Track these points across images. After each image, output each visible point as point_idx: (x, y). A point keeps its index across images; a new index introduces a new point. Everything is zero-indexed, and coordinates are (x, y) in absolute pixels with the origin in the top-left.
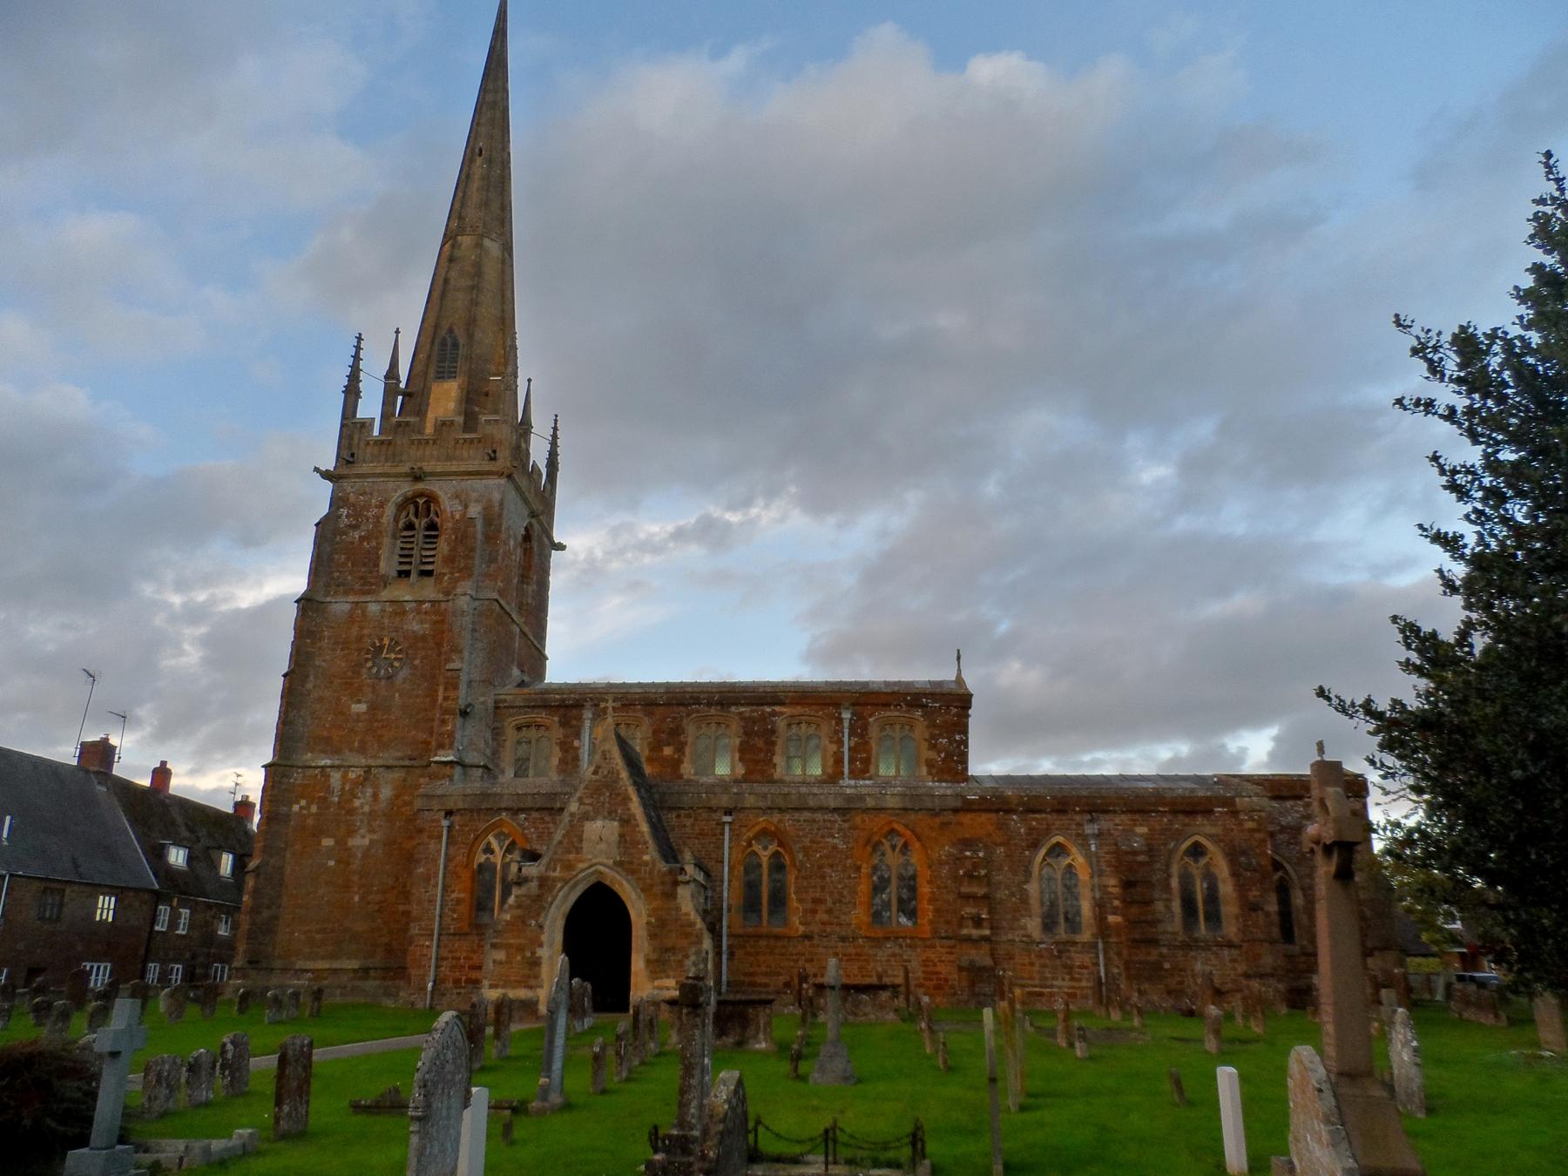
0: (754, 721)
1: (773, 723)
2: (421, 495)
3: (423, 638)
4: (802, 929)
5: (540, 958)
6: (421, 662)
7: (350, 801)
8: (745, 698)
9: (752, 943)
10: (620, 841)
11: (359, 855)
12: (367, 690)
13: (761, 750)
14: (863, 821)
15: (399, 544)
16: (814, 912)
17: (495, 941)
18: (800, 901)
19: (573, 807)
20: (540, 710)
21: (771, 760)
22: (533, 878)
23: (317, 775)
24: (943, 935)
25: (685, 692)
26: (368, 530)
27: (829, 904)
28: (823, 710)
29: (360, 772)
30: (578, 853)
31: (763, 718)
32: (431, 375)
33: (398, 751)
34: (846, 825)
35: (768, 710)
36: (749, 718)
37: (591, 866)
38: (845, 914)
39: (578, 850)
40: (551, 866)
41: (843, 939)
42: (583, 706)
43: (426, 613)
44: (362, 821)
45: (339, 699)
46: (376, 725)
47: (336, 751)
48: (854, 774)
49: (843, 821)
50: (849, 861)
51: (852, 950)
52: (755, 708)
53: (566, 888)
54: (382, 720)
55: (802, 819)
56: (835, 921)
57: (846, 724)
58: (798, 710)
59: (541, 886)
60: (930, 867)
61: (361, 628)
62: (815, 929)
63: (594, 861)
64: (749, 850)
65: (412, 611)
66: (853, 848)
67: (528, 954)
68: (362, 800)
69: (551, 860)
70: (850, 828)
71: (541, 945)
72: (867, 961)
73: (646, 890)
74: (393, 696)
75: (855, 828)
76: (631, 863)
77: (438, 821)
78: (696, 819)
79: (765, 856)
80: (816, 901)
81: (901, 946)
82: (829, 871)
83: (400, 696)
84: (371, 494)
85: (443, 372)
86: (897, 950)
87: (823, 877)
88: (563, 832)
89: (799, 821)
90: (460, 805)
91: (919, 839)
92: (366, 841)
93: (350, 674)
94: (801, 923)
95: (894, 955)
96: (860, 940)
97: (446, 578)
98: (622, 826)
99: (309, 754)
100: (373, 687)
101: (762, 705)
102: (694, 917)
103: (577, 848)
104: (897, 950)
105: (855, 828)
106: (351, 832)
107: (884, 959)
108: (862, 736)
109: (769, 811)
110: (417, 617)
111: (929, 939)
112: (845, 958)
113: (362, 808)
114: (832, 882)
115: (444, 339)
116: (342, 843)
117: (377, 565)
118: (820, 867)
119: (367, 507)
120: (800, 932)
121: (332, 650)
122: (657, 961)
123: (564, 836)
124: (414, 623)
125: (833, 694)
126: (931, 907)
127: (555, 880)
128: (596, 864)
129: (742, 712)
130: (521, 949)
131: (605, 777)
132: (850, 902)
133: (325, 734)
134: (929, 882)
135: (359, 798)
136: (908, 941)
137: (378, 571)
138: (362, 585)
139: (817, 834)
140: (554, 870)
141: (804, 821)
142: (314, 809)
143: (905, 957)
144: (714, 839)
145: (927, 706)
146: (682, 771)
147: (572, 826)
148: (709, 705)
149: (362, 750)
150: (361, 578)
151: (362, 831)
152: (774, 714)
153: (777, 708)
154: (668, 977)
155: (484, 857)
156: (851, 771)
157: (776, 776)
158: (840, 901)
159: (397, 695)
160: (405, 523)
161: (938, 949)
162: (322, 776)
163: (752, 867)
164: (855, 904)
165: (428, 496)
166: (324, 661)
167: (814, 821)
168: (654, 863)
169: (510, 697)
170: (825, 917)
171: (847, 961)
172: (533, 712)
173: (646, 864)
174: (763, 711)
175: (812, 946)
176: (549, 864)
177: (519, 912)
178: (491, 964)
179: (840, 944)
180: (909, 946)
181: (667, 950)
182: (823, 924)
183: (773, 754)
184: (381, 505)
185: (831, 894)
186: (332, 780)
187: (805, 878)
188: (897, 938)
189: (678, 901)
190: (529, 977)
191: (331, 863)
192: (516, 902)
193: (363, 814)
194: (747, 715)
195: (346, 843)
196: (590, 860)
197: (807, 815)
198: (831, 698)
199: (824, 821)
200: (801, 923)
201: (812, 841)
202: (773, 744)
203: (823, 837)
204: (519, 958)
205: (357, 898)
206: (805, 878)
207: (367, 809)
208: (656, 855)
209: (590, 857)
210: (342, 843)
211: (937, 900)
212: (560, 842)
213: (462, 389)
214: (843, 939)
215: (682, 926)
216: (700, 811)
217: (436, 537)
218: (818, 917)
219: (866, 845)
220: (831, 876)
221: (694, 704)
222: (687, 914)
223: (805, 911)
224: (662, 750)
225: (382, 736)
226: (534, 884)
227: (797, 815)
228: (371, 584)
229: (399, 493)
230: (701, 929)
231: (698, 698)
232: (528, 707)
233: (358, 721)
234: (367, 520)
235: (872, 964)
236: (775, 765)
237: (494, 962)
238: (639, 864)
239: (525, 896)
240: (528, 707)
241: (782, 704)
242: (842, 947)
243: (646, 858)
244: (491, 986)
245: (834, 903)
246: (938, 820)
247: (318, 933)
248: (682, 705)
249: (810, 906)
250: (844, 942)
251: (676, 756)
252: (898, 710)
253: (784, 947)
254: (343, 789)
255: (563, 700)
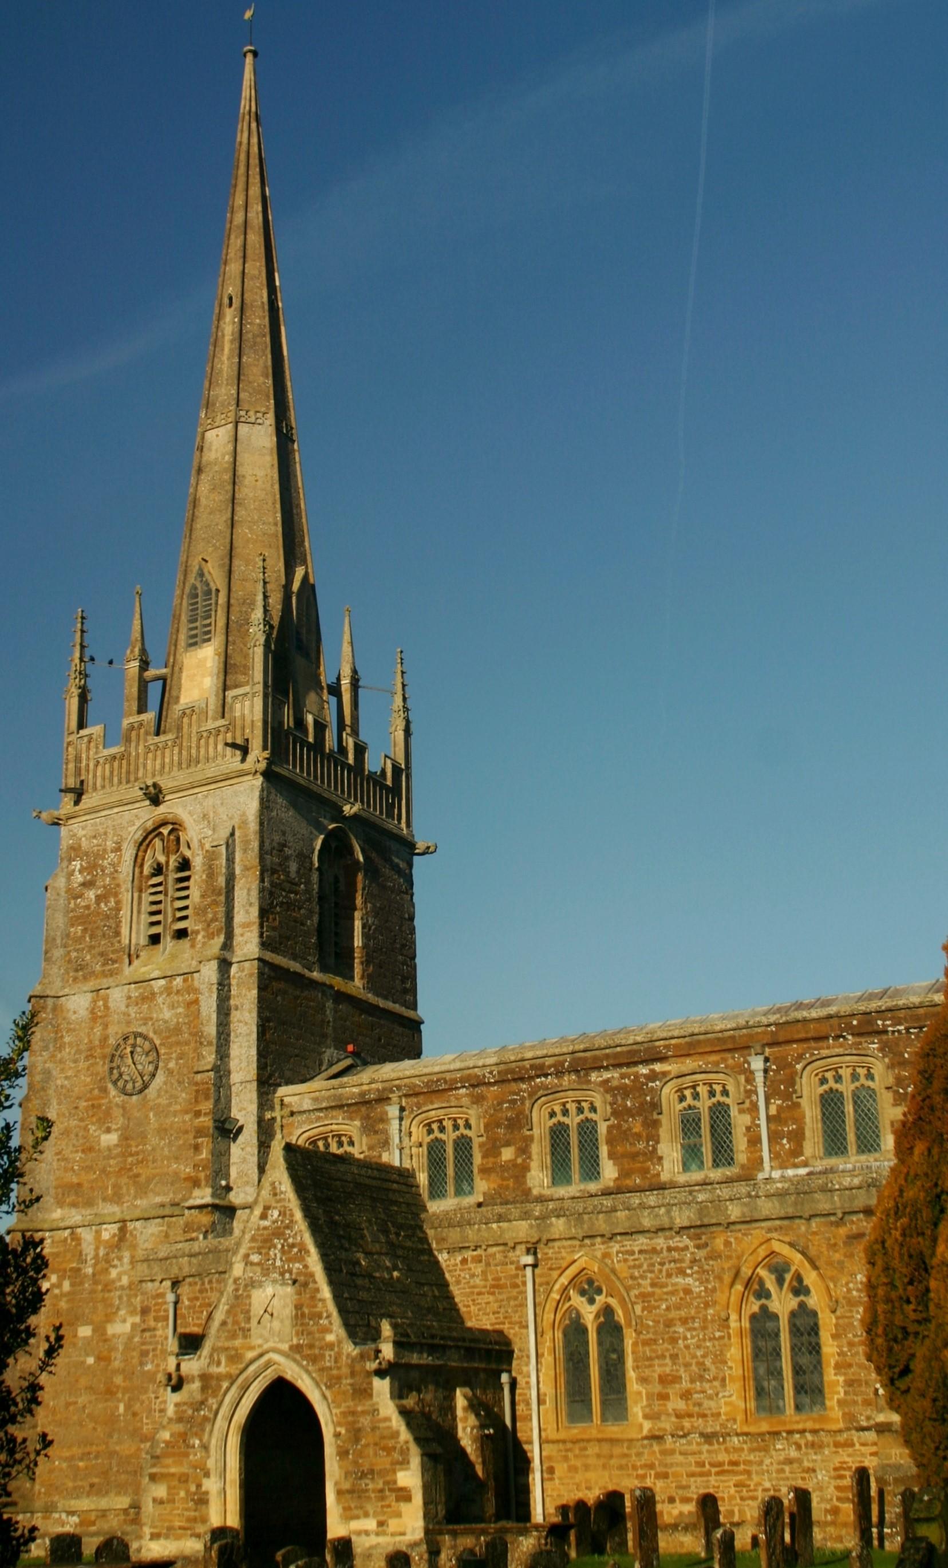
0: (624, 1091)
1: (656, 1093)
2: (164, 824)
3: (177, 1030)
4: (647, 1425)
5: (207, 1493)
6: (177, 1064)
7: (106, 1271)
8: (607, 1056)
9: (577, 1452)
10: (296, 1315)
11: (121, 1348)
12: (117, 1112)
13: (638, 1136)
14: (727, 1244)
15: (147, 898)
16: (664, 1397)
17: (154, 1470)
18: (643, 1380)
19: (238, 1269)
20: (334, 1113)
21: (655, 1149)
22: (193, 1377)
23: (66, 1239)
24: (864, 1424)
25: (523, 1060)
26: (104, 887)
27: (685, 1384)
28: (724, 1060)
29: (114, 1228)
30: (245, 1337)
31: (638, 1087)
32: (182, 637)
33: (159, 1194)
34: (701, 1254)
35: (644, 1070)
36: (617, 1088)
37: (261, 1355)
38: (710, 1398)
39: (246, 1332)
40: (214, 1361)
41: (708, 1438)
42: (389, 1099)
43: (178, 992)
44: (120, 1298)
45: (86, 1129)
46: (130, 1159)
47: (90, 1203)
48: (782, 1161)
49: (698, 1247)
50: (711, 1311)
51: (723, 1457)
52: (624, 1070)
53: (234, 1390)
54: (137, 1153)
55: (636, 1249)
56: (696, 1409)
57: (759, 1078)
58: (689, 1064)
59: (204, 1389)
60: (834, 1312)
61: (106, 1026)
62: (667, 1424)
63: (266, 1347)
64: (567, 1305)
65: (161, 993)
66: (714, 1290)
67: (193, 1488)
68: (119, 1269)
69: (214, 1350)
70: (708, 1258)
71: (207, 1475)
72: (749, 1473)
73: (332, 1382)
74: (147, 1116)
75: (714, 1256)
76: (311, 1346)
77: (162, 1295)
78: (488, 1264)
79: (589, 1314)
80: (663, 1380)
81: (799, 1447)
82: (681, 1330)
83: (154, 1116)
84: (105, 834)
85: (195, 636)
86: (793, 1453)
87: (674, 1340)
88: (226, 1307)
89: (632, 1253)
90: (186, 1271)
91: (815, 1267)
92: (127, 1327)
93: (96, 1092)
94: (646, 1417)
95: (789, 1461)
96: (735, 1439)
97: (200, 937)
98: (299, 1293)
99: (59, 1211)
100: (124, 1108)
101: (635, 1064)
102: (398, 1423)
103: (242, 1329)
104: (793, 1453)
105: (714, 1256)
106: (109, 1318)
107: (775, 1467)
108: (787, 1096)
109: (587, 1241)
110: (168, 1000)
111: (840, 1431)
112: (714, 1470)
113: (120, 1279)
114: (687, 1347)
115: (194, 587)
116: (99, 1330)
117: (118, 934)
118: (669, 1324)
119: (101, 855)
120: (645, 1432)
121: (75, 1061)
122: (351, 1492)
123: (228, 1312)
124: (165, 1010)
125: (737, 1033)
126: (841, 1379)
127: (219, 1378)
128: (267, 1352)
129: (607, 1081)
130: (184, 1479)
131: (276, 1221)
132: (715, 1379)
133: (75, 1180)
134: (834, 1337)
135: (115, 1266)
136: (809, 1436)
137: (119, 942)
138: (103, 965)
139: (660, 1271)
140: (219, 1364)
141: (641, 1252)
142: (66, 1286)
143: (806, 1464)
144: (515, 1291)
145: (886, 1032)
146: (530, 1183)
147: (237, 1297)
148: (559, 1073)
149: (117, 1198)
150: (102, 954)
151: (122, 1312)
152: (653, 1076)
153: (658, 1067)
154: (366, 1515)
155: (758, 1303)
156: (775, 1156)
157: (665, 1177)
158: (701, 1378)
159: (151, 1115)
160: (151, 866)
161: (857, 1446)
162: (72, 1240)
163: (575, 1331)
164: (723, 1380)
165: (173, 824)
166: (66, 1078)
167: (654, 1251)
168: (340, 1342)
169: (296, 1098)
170: (681, 1405)
171: (718, 1474)
172: (326, 1117)
173: (331, 1346)
174: (637, 1076)
175: (664, 1453)
176: (211, 1356)
177: (179, 1428)
178: (151, 1504)
179: (706, 1447)
180: (813, 1445)
181: (363, 1475)
182: (678, 1416)
183: (658, 1142)
184: (118, 849)
185: (687, 1365)
186: (84, 1245)
187: (646, 1343)
188: (790, 1432)
189: (375, 1399)
190: (195, 1520)
191: (90, 1360)
192: (176, 1412)
193: (122, 1288)
194: (615, 1083)
195: (105, 1330)
196: (260, 1346)
197: (642, 1242)
198: (733, 1037)
199: (670, 1249)
200: (646, 1417)
201: (653, 1285)
202: (656, 1124)
203: (669, 1275)
204: (182, 1494)
205: (122, 1408)
206: (646, 1343)
207: (125, 1281)
208: (342, 1332)
209: (260, 1341)
210: (99, 1330)
211: (850, 1366)
212: (224, 1323)
213: (218, 654)
214: (708, 1438)
215: (383, 1438)
216: (494, 1249)
217: (187, 879)
218: (670, 1406)
219: (732, 1284)
220: (685, 1338)
221: (538, 1076)
222: (388, 1419)
223: (650, 1396)
224: (500, 1154)
225: (138, 1175)
226: (196, 1385)
227: (628, 1244)
228: (114, 962)
229: (138, 824)
230: (407, 1442)
231: (541, 1067)
232: (320, 1110)
233: (109, 1157)
234: (103, 871)
235: (755, 1478)
236: (660, 1158)
237: (154, 1500)
238: (321, 1348)
239: (185, 1404)
240: (320, 1110)
241: (662, 1059)
242: (708, 1451)
243: (330, 1338)
244: (155, 1537)
245: (692, 1381)
246: (843, 1231)
247: (81, 1459)
248: (522, 1079)
249: (657, 1388)
250: (711, 1444)
251: (519, 1161)
252: (841, 1046)
253: (625, 1455)
254: (96, 1256)
255: (363, 1094)
